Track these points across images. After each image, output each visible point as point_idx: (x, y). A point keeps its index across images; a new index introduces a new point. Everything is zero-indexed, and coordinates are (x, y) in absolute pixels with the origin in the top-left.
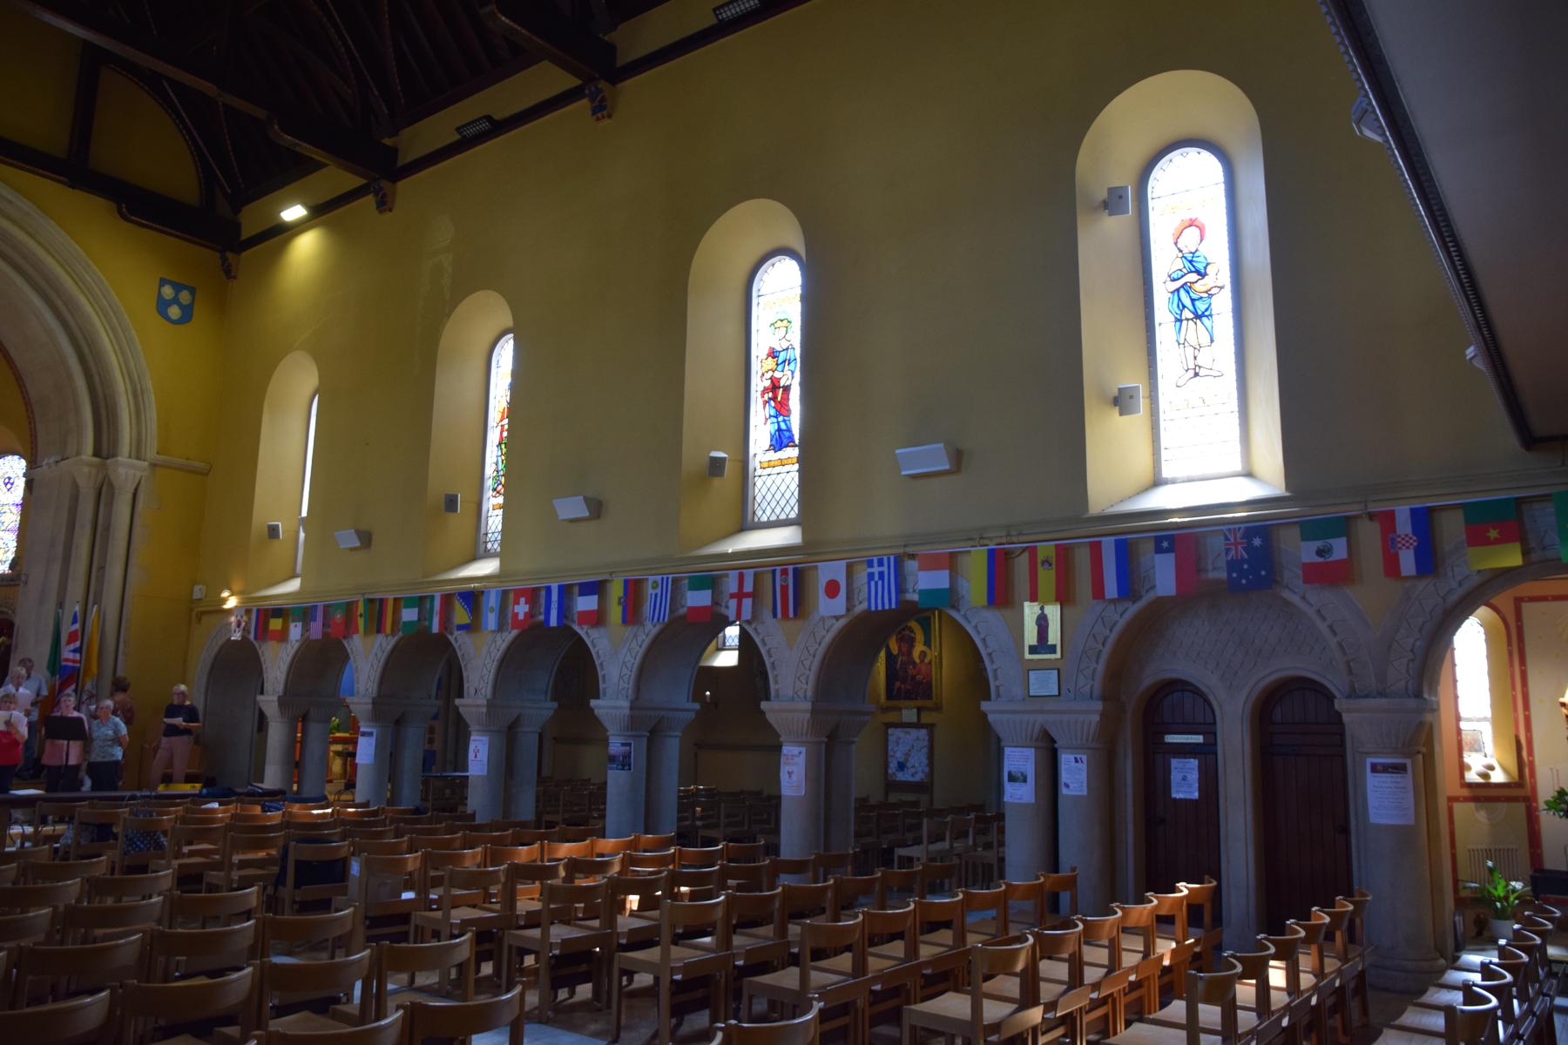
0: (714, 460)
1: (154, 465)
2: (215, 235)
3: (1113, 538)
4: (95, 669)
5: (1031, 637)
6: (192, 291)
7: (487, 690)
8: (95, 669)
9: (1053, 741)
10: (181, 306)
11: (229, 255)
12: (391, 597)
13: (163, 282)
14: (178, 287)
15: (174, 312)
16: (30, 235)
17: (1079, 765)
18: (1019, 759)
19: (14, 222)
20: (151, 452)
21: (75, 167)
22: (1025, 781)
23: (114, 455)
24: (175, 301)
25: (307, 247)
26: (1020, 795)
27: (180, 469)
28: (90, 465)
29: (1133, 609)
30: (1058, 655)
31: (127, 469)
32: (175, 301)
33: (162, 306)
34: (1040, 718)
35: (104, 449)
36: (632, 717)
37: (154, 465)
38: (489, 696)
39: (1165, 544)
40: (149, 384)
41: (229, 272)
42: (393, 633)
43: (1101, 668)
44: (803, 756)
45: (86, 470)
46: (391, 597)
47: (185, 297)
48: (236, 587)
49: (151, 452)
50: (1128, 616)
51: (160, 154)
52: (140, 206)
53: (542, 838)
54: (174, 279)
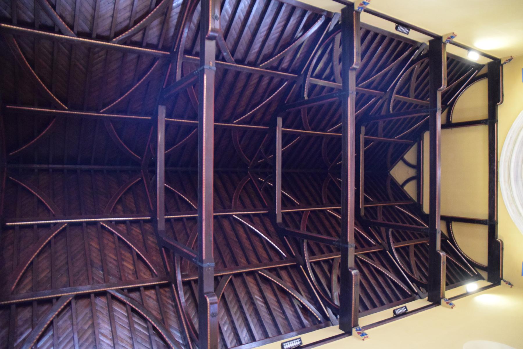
11: (502, 63)
21: (491, 121)
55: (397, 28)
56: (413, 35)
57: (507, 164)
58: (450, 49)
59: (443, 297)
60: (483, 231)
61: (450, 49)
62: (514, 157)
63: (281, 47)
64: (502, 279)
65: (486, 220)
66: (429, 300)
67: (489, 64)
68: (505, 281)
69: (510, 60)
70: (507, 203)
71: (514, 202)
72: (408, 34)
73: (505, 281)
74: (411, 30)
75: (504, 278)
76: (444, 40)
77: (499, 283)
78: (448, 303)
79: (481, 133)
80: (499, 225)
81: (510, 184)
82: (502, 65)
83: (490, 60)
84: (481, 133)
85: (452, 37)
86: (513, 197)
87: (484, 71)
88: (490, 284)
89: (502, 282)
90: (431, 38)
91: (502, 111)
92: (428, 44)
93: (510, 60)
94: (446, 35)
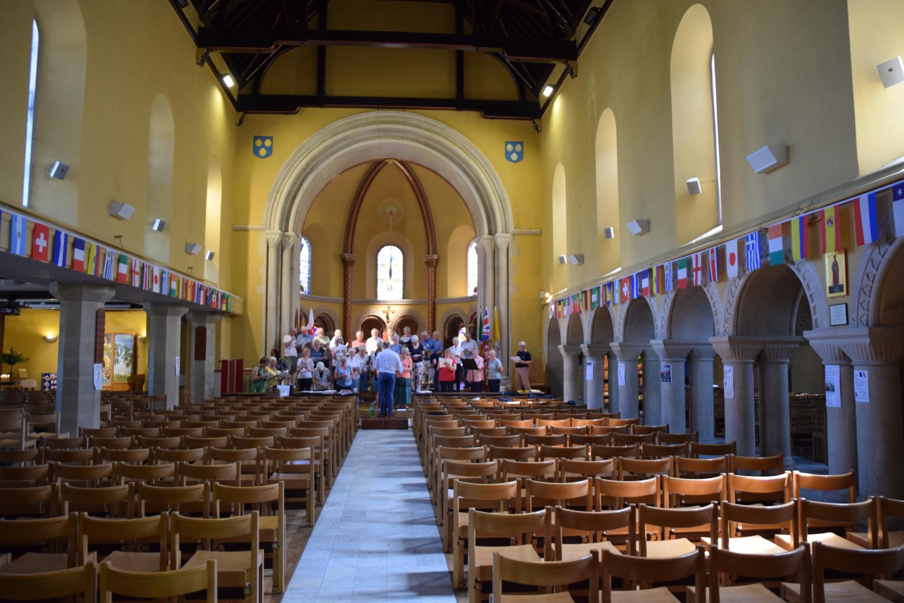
0: (689, 184)
1: (514, 235)
2: (528, 111)
3: (866, 195)
4: (498, 336)
5: (829, 282)
6: (522, 144)
7: (621, 339)
8: (498, 336)
9: (850, 360)
10: (517, 153)
11: (536, 120)
12: (588, 289)
13: (507, 143)
14: (514, 144)
15: (514, 157)
16: (446, 138)
17: (863, 378)
18: (833, 374)
19: (439, 134)
20: (511, 229)
21: (459, 101)
22: (833, 390)
23: (496, 232)
24: (514, 151)
25: (558, 107)
26: (833, 400)
27: (526, 234)
28: (487, 239)
29: (890, 249)
30: (844, 293)
31: (502, 239)
32: (514, 151)
33: (508, 155)
34: (837, 342)
35: (492, 232)
36: (666, 350)
37: (514, 235)
38: (665, 336)
39: (900, 192)
40: (506, 195)
41: (537, 129)
42: (592, 309)
43: (872, 300)
44: (732, 372)
45: (486, 242)
46: (588, 289)
47: (518, 148)
48: (551, 291)
49: (511, 229)
50: (887, 256)
51: (494, 79)
52: (492, 109)
53: (571, 417)
54: (513, 140)
55: (594, 9)
56: (583, 28)
57: (402, 120)
58: (560, 67)
59: (209, 51)
60: (308, 88)
61: (560, 67)
62: (410, 128)
63: (288, 561)
64: (245, 113)
65: (324, 92)
66: (200, 28)
67: (538, 104)
68: (243, 116)
69: (537, 129)
70: (348, 120)
71: (351, 128)
72: (585, 21)
73: (243, 116)
74: (589, 26)
75: (247, 115)
76: (571, 63)
77: (238, 110)
78: (203, 56)
79: (443, 86)
80: (318, 109)
81: (374, 123)
82: (533, 120)
83: (542, 105)
84: (443, 86)
85: (572, 74)
86: (357, 126)
87: (530, 96)
88: (236, 98)
89: (242, 113)
90: (578, 43)
91: (470, 117)
92: (572, 39)
93: (537, 129)
94: (577, 66)
